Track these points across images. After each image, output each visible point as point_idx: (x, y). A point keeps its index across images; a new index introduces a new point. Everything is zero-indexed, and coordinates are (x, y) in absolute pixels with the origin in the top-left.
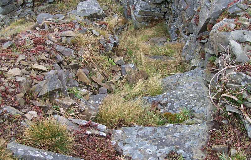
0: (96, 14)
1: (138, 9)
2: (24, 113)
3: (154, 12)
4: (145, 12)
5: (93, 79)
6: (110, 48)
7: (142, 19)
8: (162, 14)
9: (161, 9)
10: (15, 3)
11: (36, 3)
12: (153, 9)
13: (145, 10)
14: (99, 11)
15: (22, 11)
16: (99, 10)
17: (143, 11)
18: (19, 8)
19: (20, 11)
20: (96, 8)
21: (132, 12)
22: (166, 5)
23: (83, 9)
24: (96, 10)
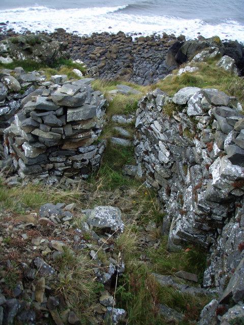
0: (109, 228)
1: (179, 228)
2: (18, 160)
3: (196, 238)
4: (186, 235)
5: (53, 315)
6: (104, 279)
7: (180, 241)
8: (206, 244)
9: (206, 238)
10: (43, 165)
11: (66, 173)
12: (196, 234)
13: (185, 233)
14: (114, 226)
15: (47, 177)
16: (115, 224)
17: (183, 233)
18: (45, 173)
19: (44, 176)
20: (113, 221)
21: (171, 228)
22: (214, 234)
23: (97, 216)
24: (111, 224)
